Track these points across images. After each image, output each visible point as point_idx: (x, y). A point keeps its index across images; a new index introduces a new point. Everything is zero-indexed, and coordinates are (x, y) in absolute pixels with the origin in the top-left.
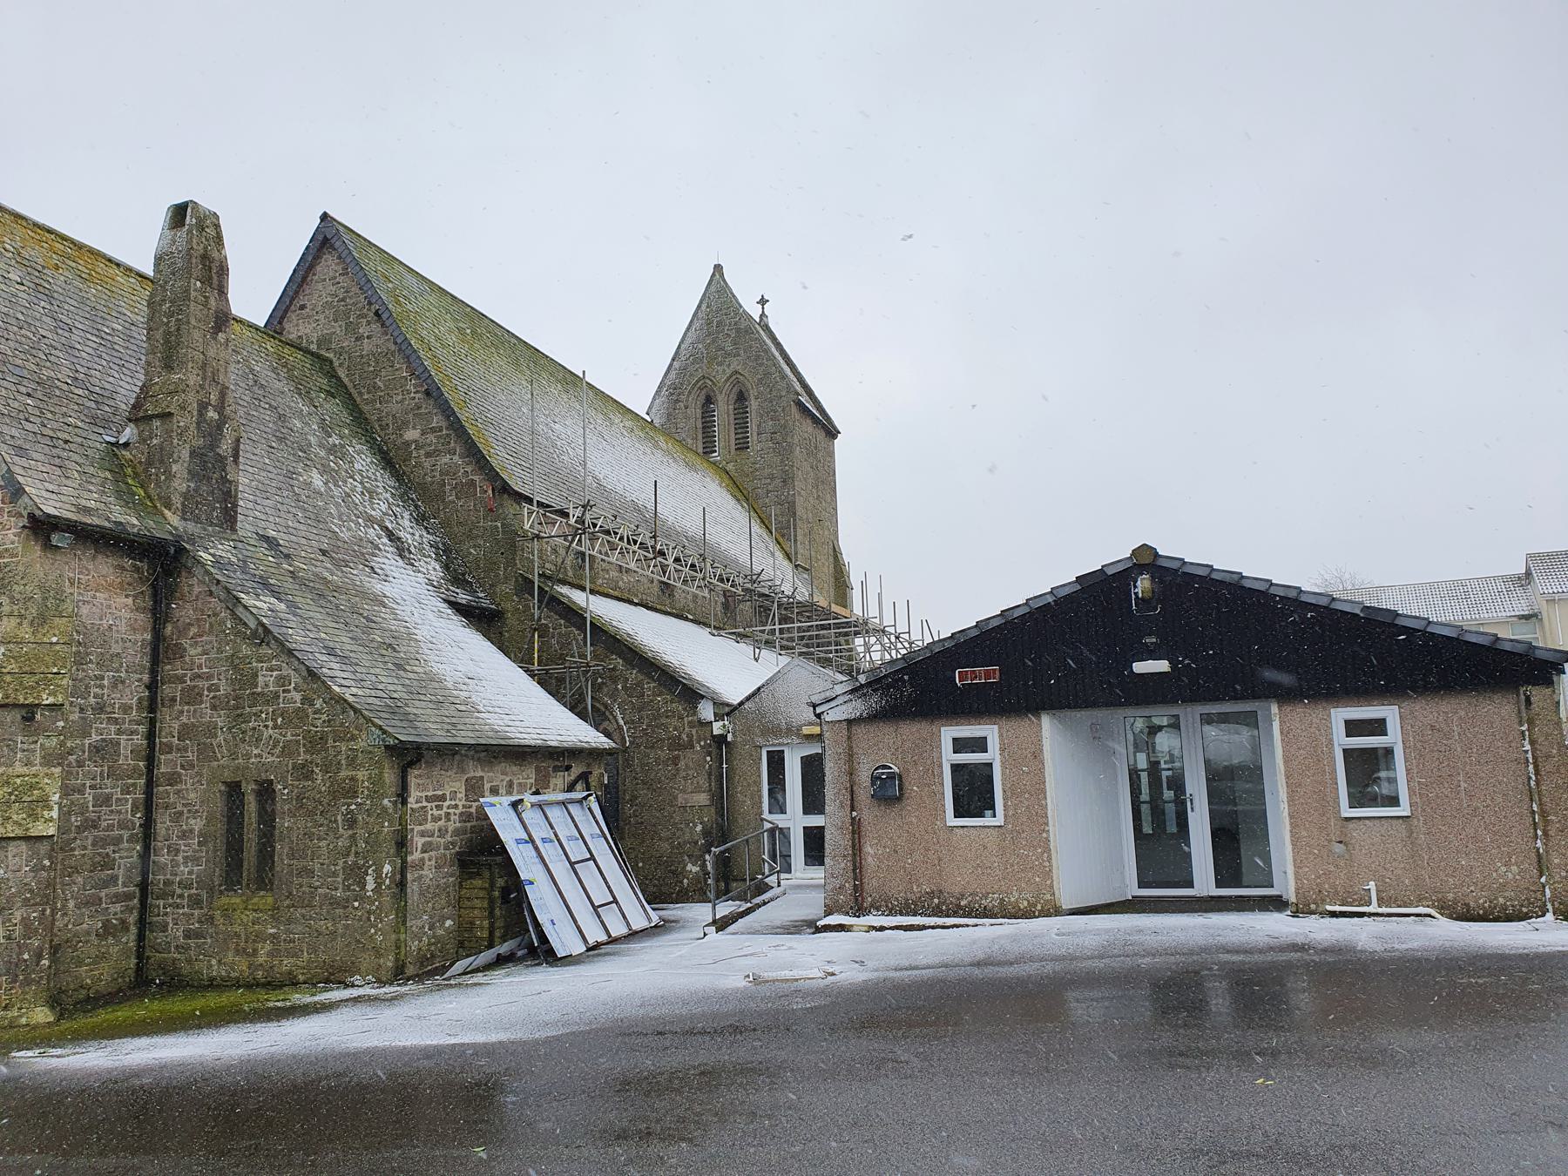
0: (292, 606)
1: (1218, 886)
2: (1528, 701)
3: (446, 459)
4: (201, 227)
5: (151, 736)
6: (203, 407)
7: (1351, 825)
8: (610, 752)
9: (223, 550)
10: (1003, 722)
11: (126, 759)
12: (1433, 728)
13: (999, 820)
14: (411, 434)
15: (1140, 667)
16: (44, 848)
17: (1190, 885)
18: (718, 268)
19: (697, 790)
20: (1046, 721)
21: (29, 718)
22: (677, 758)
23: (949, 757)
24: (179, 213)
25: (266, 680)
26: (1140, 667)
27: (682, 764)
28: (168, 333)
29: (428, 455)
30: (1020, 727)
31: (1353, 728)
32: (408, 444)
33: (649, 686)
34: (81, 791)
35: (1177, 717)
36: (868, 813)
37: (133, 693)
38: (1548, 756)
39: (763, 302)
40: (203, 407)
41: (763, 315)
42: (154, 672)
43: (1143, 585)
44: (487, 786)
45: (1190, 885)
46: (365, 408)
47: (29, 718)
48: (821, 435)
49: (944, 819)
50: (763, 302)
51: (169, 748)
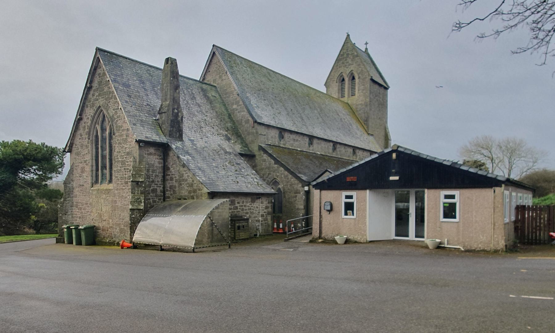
0: (193, 157)
1: (416, 237)
2: (494, 192)
3: (242, 113)
4: (172, 63)
5: (164, 188)
6: (174, 109)
7: (443, 223)
8: (275, 194)
9: (179, 144)
10: (357, 191)
11: (159, 193)
12: (468, 198)
13: (355, 217)
14: (235, 107)
15: (392, 178)
16: (141, 211)
17: (407, 236)
18: (348, 35)
19: (301, 205)
20: (368, 191)
21: (138, 184)
22: (296, 196)
23: (344, 200)
24: (167, 60)
25: (185, 176)
26: (392, 178)
27: (297, 198)
28: (166, 92)
29: (239, 112)
30: (361, 192)
31: (447, 197)
32: (234, 109)
33: (290, 176)
34: (150, 199)
35: (409, 191)
36: (325, 214)
37: (160, 179)
38: (498, 207)
39: (366, 44)
40: (174, 109)
41: (366, 49)
42: (164, 173)
43: (394, 155)
44: (236, 202)
45: (407, 236)
46: (224, 99)
47: (138, 184)
48: (382, 90)
49: (439, 219)
50: (366, 44)
51: (167, 191)
